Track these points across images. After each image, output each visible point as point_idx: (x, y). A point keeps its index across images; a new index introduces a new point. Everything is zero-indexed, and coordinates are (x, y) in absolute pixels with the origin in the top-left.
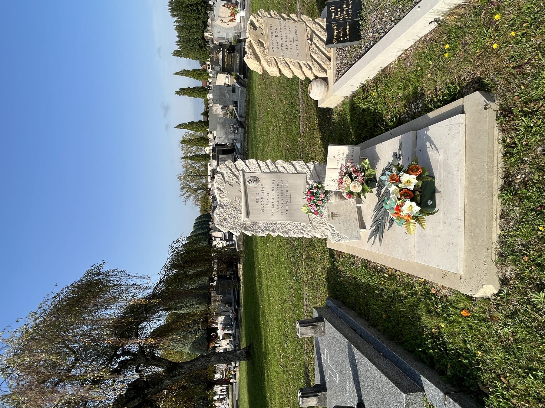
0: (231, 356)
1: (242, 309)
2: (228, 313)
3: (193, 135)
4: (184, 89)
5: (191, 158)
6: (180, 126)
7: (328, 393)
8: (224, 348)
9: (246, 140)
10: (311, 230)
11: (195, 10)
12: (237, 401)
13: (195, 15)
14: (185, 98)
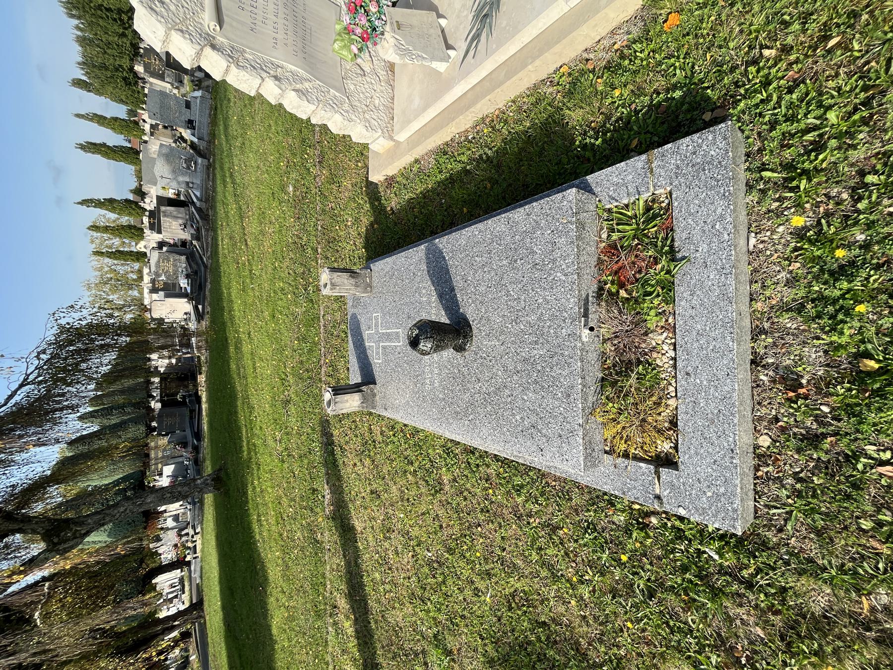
0: (186, 489)
1: (206, 443)
2: (181, 459)
3: (114, 221)
4: (95, 144)
5: (110, 255)
6: (85, 202)
7: (377, 388)
8: (174, 513)
9: (211, 177)
10: (347, 108)
11: (115, 20)
12: (198, 585)
13: (115, 27)
14: (98, 159)
